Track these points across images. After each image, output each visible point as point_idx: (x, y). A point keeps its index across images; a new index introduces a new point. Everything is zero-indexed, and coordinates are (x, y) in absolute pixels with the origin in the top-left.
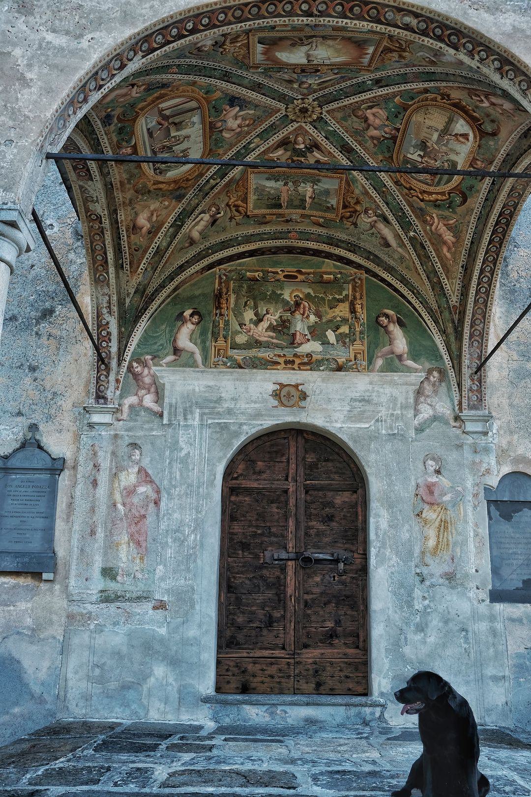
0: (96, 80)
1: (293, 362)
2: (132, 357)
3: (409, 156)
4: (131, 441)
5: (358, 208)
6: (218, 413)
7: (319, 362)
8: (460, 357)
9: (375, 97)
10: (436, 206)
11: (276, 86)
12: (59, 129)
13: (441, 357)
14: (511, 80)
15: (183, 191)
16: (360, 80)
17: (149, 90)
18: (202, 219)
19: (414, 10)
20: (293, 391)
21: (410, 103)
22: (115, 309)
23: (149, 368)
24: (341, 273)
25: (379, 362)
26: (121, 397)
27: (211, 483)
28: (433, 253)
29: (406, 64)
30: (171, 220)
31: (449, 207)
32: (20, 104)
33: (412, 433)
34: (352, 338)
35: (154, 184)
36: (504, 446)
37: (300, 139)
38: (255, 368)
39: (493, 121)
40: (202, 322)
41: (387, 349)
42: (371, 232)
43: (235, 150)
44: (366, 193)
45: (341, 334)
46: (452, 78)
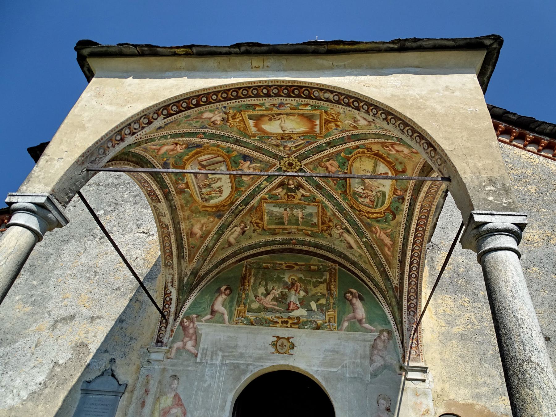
0: (130, 128)
1: (287, 322)
2: (184, 315)
3: (356, 189)
4: (173, 374)
5: (331, 224)
6: (234, 356)
7: (305, 323)
8: (401, 322)
9: (329, 154)
10: (377, 221)
11: (270, 149)
12: (99, 154)
13: (389, 322)
14: (394, 124)
15: (222, 213)
16: (319, 143)
17: (189, 148)
18: (235, 230)
19: (330, 89)
20: (285, 342)
21: (350, 156)
22: (176, 283)
23: (194, 323)
24: (322, 265)
25: (346, 324)
26: (173, 342)
27: (223, 408)
28: (379, 252)
29: (341, 131)
30: (215, 230)
31: (385, 222)
32: (76, 139)
33: (368, 377)
34: (327, 307)
35: (202, 207)
36: (438, 391)
37: (291, 182)
38: (262, 325)
39: (401, 163)
40: (231, 295)
41: (351, 315)
42: (340, 239)
43: (252, 188)
44: (335, 215)
45: (320, 304)
46: (369, 136)
